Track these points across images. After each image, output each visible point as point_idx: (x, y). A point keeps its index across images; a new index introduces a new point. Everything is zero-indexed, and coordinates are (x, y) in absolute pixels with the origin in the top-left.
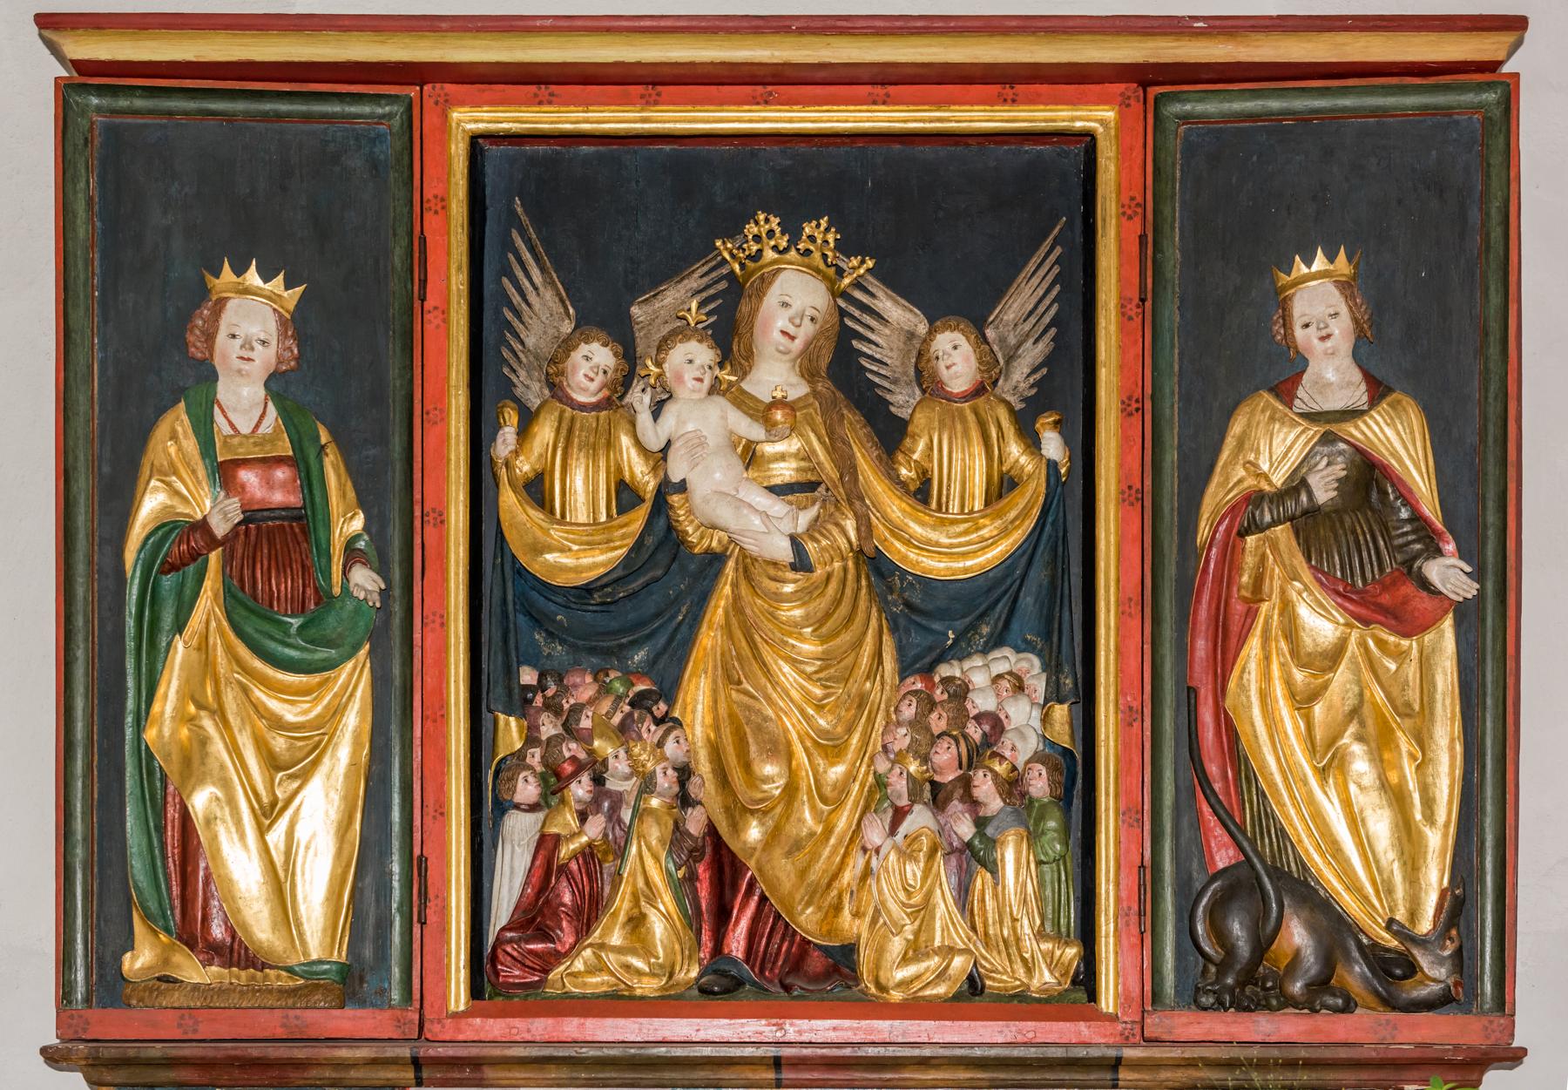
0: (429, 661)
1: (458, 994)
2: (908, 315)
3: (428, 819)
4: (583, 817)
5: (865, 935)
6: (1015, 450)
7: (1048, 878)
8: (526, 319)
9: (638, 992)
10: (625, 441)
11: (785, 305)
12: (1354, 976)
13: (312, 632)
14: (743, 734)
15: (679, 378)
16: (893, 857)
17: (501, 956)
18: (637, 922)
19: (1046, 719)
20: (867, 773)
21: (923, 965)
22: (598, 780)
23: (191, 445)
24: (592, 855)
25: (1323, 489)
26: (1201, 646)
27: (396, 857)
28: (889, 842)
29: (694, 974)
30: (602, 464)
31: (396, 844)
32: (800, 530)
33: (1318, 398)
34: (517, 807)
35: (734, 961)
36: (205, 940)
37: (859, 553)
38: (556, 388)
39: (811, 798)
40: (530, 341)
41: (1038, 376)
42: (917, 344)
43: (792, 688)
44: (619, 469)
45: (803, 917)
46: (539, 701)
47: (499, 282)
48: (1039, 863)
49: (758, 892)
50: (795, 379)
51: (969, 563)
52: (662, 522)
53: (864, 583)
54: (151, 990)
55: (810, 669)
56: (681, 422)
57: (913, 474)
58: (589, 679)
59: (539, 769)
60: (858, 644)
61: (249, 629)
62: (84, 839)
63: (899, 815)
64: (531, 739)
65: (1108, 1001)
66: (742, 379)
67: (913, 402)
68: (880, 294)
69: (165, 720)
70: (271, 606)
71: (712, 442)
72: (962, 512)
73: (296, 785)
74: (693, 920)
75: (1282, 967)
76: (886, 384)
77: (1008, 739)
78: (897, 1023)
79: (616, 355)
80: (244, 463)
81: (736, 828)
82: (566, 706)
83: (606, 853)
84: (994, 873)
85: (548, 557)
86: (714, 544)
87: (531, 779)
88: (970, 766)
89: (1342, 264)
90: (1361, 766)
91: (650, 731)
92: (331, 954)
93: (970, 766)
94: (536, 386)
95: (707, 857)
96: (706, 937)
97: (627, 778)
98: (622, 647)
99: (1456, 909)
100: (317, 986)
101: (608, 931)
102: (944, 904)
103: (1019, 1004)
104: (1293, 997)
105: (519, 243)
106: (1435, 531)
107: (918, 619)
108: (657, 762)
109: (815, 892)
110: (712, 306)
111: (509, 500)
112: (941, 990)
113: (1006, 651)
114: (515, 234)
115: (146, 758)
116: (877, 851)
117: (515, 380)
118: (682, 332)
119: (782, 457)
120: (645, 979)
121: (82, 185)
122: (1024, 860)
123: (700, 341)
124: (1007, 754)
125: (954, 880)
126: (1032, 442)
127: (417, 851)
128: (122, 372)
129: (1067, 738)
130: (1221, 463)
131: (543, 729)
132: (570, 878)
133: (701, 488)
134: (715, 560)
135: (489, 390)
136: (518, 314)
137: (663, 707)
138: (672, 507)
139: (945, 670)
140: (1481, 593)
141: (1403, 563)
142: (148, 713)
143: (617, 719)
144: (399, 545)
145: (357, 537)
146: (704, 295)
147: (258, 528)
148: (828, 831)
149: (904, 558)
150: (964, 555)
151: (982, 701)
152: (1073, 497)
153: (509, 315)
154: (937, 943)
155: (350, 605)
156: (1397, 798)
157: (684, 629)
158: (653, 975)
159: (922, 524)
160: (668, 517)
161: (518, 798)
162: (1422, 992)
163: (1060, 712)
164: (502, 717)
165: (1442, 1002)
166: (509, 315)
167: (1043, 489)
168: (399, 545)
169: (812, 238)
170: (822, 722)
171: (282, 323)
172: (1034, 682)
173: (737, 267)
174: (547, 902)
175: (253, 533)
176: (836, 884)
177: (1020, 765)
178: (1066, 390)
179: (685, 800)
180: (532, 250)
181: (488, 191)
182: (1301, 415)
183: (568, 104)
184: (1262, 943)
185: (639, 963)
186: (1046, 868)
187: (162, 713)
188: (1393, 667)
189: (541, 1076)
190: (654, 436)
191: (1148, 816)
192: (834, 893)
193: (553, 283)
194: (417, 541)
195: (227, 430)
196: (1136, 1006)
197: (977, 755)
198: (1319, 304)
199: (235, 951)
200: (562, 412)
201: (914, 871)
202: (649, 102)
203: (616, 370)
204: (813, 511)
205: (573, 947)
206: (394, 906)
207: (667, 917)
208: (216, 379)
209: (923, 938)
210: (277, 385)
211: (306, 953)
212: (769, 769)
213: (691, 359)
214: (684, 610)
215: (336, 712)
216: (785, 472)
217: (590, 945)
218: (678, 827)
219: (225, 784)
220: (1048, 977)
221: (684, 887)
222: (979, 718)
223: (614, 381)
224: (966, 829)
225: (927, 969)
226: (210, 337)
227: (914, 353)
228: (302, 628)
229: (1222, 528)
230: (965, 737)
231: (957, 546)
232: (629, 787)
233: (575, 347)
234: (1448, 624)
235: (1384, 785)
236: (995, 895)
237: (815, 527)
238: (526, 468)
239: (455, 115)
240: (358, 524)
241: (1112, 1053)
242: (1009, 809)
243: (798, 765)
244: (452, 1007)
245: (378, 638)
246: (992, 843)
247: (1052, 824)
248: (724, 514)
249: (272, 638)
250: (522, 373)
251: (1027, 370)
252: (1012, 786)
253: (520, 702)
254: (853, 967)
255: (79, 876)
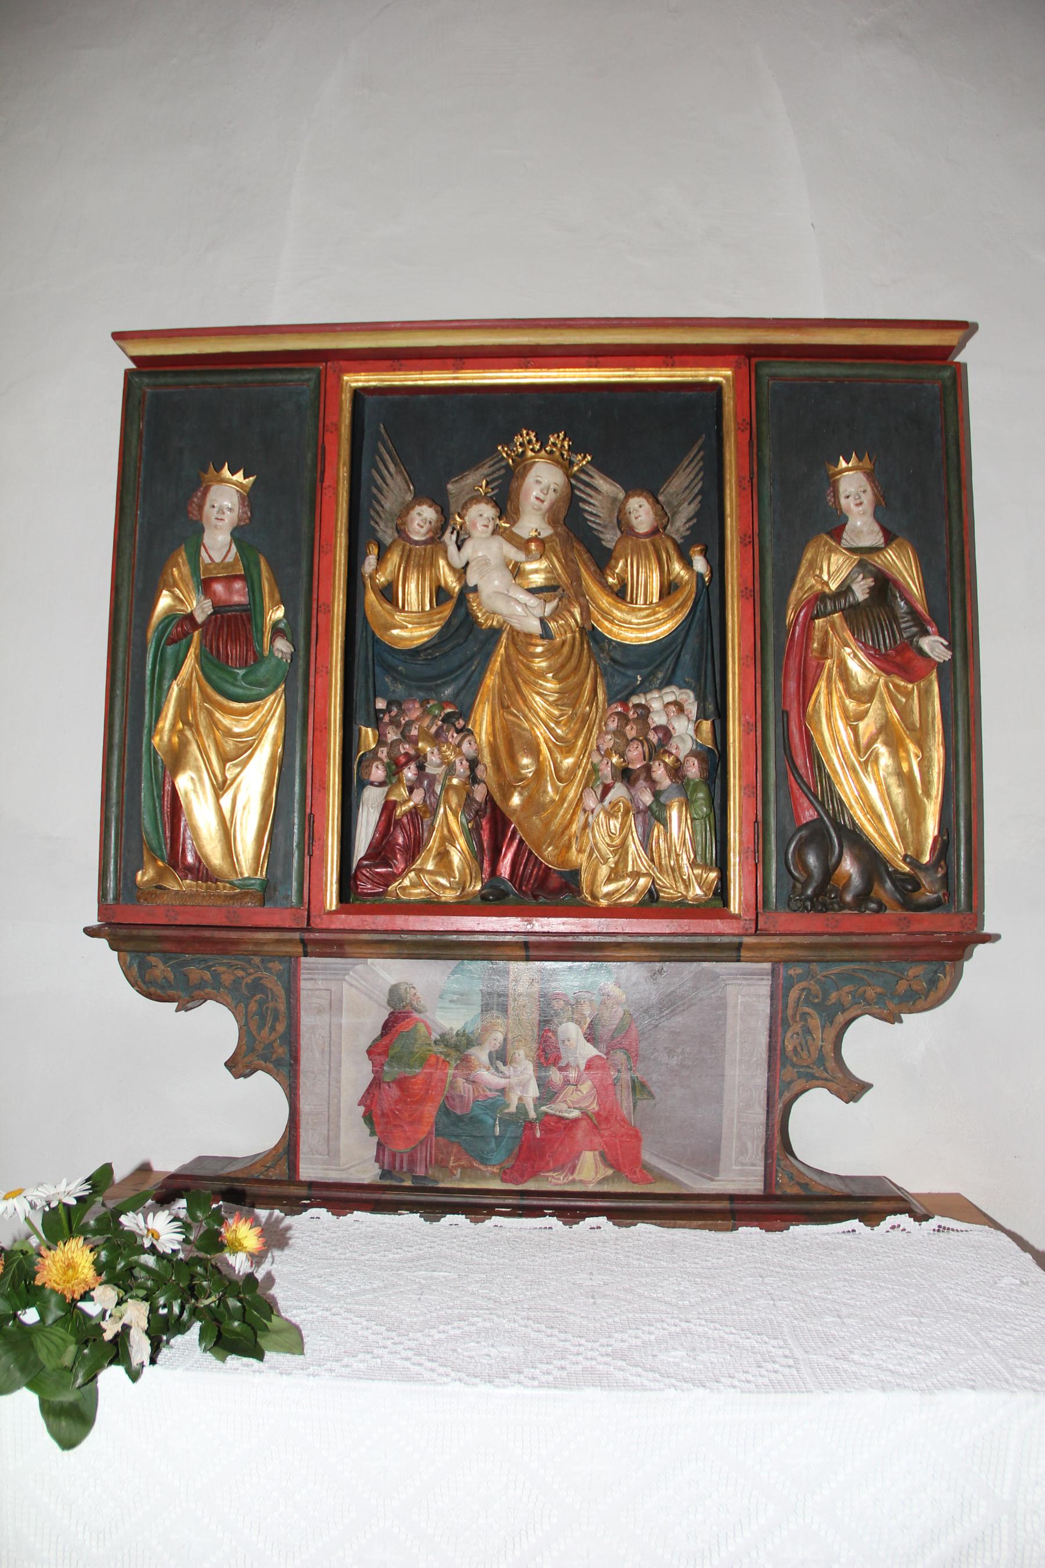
0: (318, 695)
1: (331, 900)
2: (613, 488)
3: (315, 792)
4: (411, 790)
5: (584, 864)
6: (677, 568)
7: (698, 829)
8: (385, 493)
9: (443, 899)
10: (442, 562)
11: (538, 482)
12: (885, 890)
13: (251, 678)
14: (512, 741)
15: (474, 525)
16: (602, 815)
17: (360, 876)
18: (443, 856)
19: (697, 730)
20: (587, 763)
21: (621, 883)
22: (421, 768)
23: (186, 570)
24: (417, 814)
25: (861, 591)
26: (792, 685)
27: (296, 814)
28: (600, 806)
29: (478, 888)
30: (427, 576)
31: (296, 806)
32: (546, 614)
33: (855, 539)
34: (372, 784)
35: (502, 880)
36: (183, 863)
37: (582, 629)
38: (401, 532)
39: (552, 778)
40: (387, 506)
41: (691, 524)
42: (618, 504)
43: (542, 705)
44: (438, 580)
45: (546, 853)
46: (387, 719)
47: (370, 472)
48: (693, 820)
49: (518, 837)
50: (544, 525)
51: (649, 634)
52: (463, 610)
53: (585, 646)
54: (151, 894)
55: (551, 699)
56: (475, 551)
57: (615, 581)
58: (417, 705)
59: (386, 760)
60: (582, 683)
61: (214, 677)
62: (118, 803)
63: (607, 789)
64: (381, 742)
65: (734, 907)
66: (513, 525)
67: (616, 538)
68: (596, 476)
69: (164, 732)
70: (227, 662)
71: (493, 562)
72: (645, 604)
73: (238, 770)
74: (478, 854)
75: (841, 885)
76: (599, 528)
77: (674, 742)
78: (603, 920)
79: (437, 512)
80: (217, 579)
81: (507, 797)
82: (403, 722)
83: (425, 812)
84: (665, 826)
85: (395, 632)
86: (495, 623)
87: (380, 766)
88: (650, 759)
89: (867, 463)
90: (885, 759)
91: (454, 737)
92: (256, 874)
93: (650, 759)
94: (390, 531)
95: (488, 815)
96: (486, 865)
97: (439, 766)
98: (438, 686)
99: (944, 845)
100: (247, 893)
101: (425, 861)
102: (634, 846)
103: (680, 909)
104: (848, 903)
105: (383, 450)
106: (925, 620)
107: (620, 669)
108: (457, 755)
109: (554, 837)
110: (496, 484)
111: (371, 597)
112: (631, 899)
113: (673, 688)
114: (380, 446)
115: (153, 753)
116: (592, 812)
117: (377, 528)
118: (476, 499)
119: (536, 571)
120: (448, 891)
121: (136, 427)
122: (684, 818)
123: (487, 503)
124: (674, 751)
125: (640, 830)
126: (688, 564)
127: (308, 811)
128: (150, 524)
129: (710, 742)
130: (800, 576)
131: (389, 736)
132: (403, 827)
133: (485, 590)
134: (495, 633)
135: (363, 533)
136: (380, 491)
137: (462, 722)
138: (469, 601)
139: (635, 700)
140: (953, 659)
141: (908, 638)
142: (155, 727)
143: (433, 730)
144: (305, 628)
145: (279, 621)
146: (491, 477)
147: (222, 617)
148: (563, 799)
149: (610, 632)
150: (647, 630)
151: (658, 719)
152: (710, 598)
153: (375, 491)
154: (630, 869)
155: (274, 662)
156: (905, 779)
157: (476, 674)
158: (451, 888)
159: (621, 610)
160: (467, 608)
161: (373, 778)
162: (923, 900)
163: (706, 725)
164: (363, 728)
165: (936, 904)
166: (375, 491)
167: (694, 589)
168: (305, 628)
169: (554, 444)
170: (559, 731)
171: (242, 498)
172: (690, 707)
173: (510, 461)
174: (388, 842)
175: (219, 620)
176: (567, 832)
177: (681, 757)
178: (707, 534)
179: (473, 779)
180: (389, 453)
181: (366, 420)
182: (846, 549)
183: (411, 370)
184: (829, 871)
185: (443, 881)
186: (697, 822)
187: (163, 727)
188: (904, 700)
189: (379, 952)
190: (458, 559)
191: (758, 791)
192: (566, 838)
193: (401, 472)
194: (314, 623)
195: (207, 560)
196: (752, 910)
197: (656, 752)
198: (853, 487)
199: (201, 871)
200: (404, 546)
201: (615, 824)
202: (457, 368)
203: (437, 521)
204: (555, 603)
205: (403, 870)
206: (295, 844)
207: (462, 852)
208: (203, 531)
209: (621, 866)
210: (238, 535)
211: (242, 874)
212: (525, 761)
213: (481, 515)
214: (476, 663)
215: (263, 726)
216: (538, 580)
217: (414, 870)
218: (469, 799)
219: (198, 770)
220: (699, 892)
221: (473, 833)
222: (656, 729)
223: (436, 528)
224: (647, 798)
225: (623, 886)
226: (201, 507)
227: (617, 510)
228: (244, 676)
229: (802, 614)
230: (648, 741)
231: (641, 624)
232: (439, 771)
233: (413, 508)
234: (934, 676)
235: (899, 774)
236: (666, 840)
237: (555, 614)
238: (382, 579)
239: (345, 378)
240: (279, 613)
241: (736, 940)
242: (675, 785)
243: (545, 758)
244: (328, 907)
245: (288, 680)
246: (665, 807)
247: (701, 795)
248: (500, 606)
249: (227, 681)
250: (382, 525)
251: (684, 520)
252: (676, 771)
253: (376, 721)
254: (578, 883)
255: (113, 824)
